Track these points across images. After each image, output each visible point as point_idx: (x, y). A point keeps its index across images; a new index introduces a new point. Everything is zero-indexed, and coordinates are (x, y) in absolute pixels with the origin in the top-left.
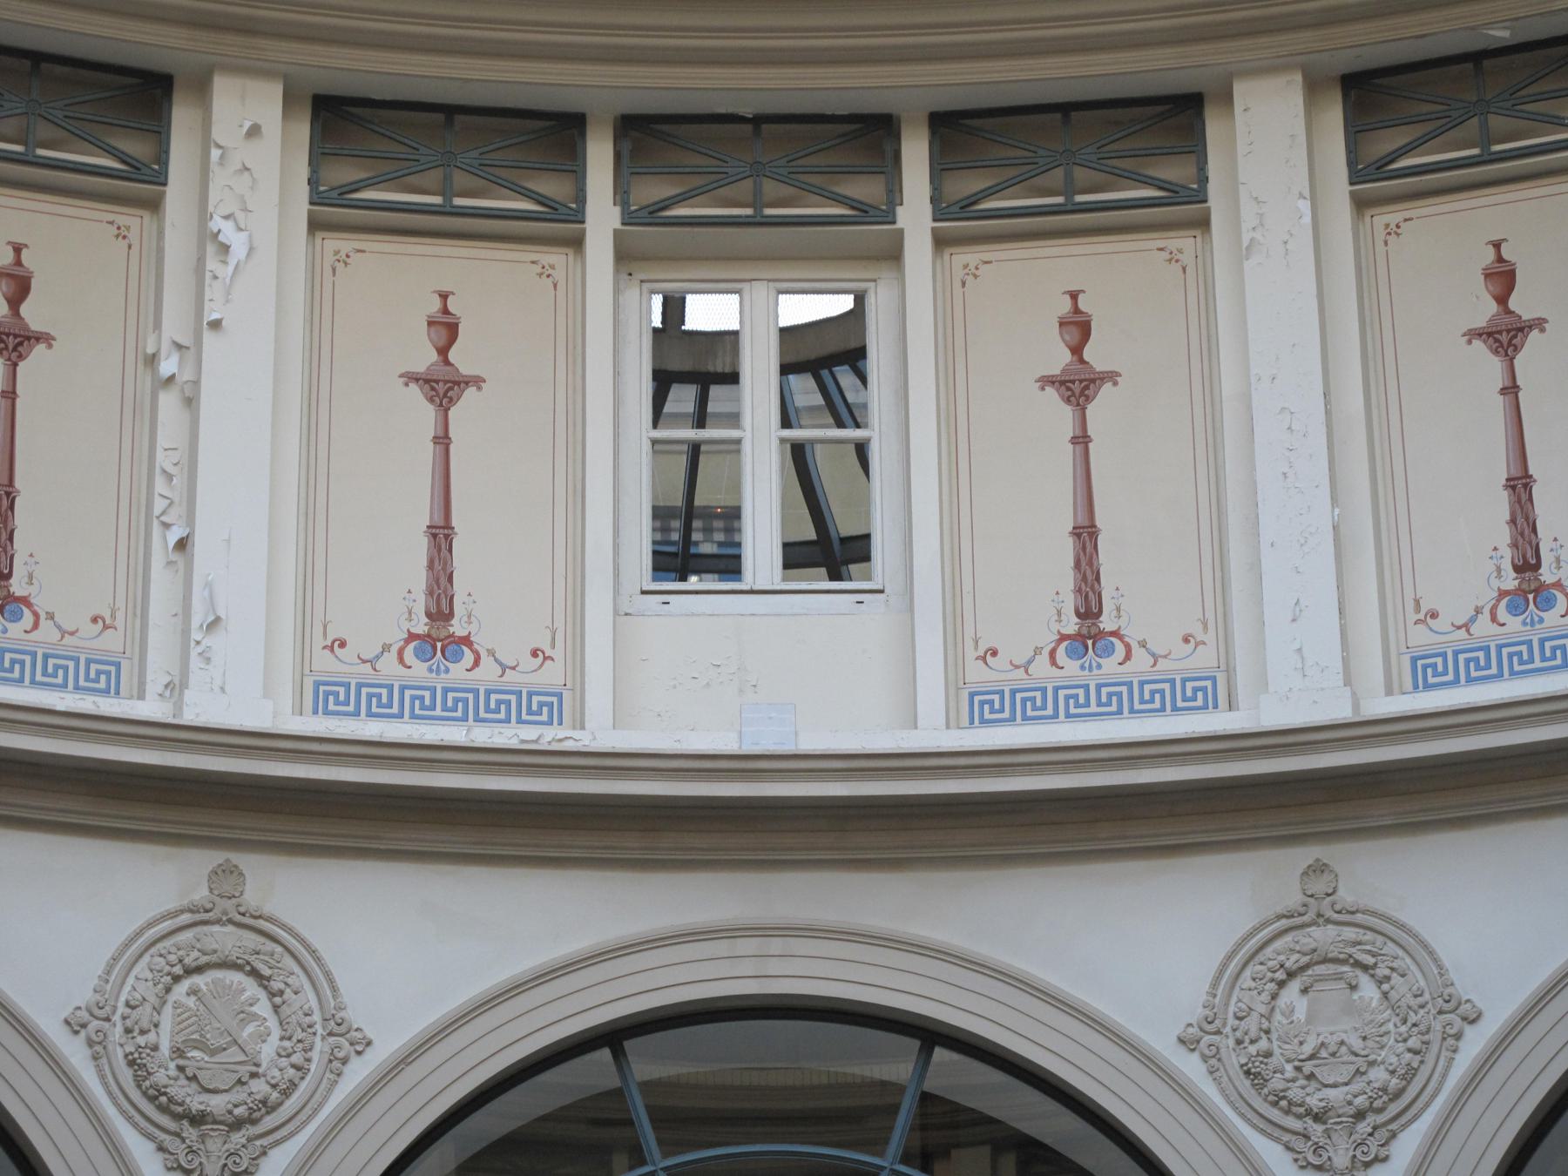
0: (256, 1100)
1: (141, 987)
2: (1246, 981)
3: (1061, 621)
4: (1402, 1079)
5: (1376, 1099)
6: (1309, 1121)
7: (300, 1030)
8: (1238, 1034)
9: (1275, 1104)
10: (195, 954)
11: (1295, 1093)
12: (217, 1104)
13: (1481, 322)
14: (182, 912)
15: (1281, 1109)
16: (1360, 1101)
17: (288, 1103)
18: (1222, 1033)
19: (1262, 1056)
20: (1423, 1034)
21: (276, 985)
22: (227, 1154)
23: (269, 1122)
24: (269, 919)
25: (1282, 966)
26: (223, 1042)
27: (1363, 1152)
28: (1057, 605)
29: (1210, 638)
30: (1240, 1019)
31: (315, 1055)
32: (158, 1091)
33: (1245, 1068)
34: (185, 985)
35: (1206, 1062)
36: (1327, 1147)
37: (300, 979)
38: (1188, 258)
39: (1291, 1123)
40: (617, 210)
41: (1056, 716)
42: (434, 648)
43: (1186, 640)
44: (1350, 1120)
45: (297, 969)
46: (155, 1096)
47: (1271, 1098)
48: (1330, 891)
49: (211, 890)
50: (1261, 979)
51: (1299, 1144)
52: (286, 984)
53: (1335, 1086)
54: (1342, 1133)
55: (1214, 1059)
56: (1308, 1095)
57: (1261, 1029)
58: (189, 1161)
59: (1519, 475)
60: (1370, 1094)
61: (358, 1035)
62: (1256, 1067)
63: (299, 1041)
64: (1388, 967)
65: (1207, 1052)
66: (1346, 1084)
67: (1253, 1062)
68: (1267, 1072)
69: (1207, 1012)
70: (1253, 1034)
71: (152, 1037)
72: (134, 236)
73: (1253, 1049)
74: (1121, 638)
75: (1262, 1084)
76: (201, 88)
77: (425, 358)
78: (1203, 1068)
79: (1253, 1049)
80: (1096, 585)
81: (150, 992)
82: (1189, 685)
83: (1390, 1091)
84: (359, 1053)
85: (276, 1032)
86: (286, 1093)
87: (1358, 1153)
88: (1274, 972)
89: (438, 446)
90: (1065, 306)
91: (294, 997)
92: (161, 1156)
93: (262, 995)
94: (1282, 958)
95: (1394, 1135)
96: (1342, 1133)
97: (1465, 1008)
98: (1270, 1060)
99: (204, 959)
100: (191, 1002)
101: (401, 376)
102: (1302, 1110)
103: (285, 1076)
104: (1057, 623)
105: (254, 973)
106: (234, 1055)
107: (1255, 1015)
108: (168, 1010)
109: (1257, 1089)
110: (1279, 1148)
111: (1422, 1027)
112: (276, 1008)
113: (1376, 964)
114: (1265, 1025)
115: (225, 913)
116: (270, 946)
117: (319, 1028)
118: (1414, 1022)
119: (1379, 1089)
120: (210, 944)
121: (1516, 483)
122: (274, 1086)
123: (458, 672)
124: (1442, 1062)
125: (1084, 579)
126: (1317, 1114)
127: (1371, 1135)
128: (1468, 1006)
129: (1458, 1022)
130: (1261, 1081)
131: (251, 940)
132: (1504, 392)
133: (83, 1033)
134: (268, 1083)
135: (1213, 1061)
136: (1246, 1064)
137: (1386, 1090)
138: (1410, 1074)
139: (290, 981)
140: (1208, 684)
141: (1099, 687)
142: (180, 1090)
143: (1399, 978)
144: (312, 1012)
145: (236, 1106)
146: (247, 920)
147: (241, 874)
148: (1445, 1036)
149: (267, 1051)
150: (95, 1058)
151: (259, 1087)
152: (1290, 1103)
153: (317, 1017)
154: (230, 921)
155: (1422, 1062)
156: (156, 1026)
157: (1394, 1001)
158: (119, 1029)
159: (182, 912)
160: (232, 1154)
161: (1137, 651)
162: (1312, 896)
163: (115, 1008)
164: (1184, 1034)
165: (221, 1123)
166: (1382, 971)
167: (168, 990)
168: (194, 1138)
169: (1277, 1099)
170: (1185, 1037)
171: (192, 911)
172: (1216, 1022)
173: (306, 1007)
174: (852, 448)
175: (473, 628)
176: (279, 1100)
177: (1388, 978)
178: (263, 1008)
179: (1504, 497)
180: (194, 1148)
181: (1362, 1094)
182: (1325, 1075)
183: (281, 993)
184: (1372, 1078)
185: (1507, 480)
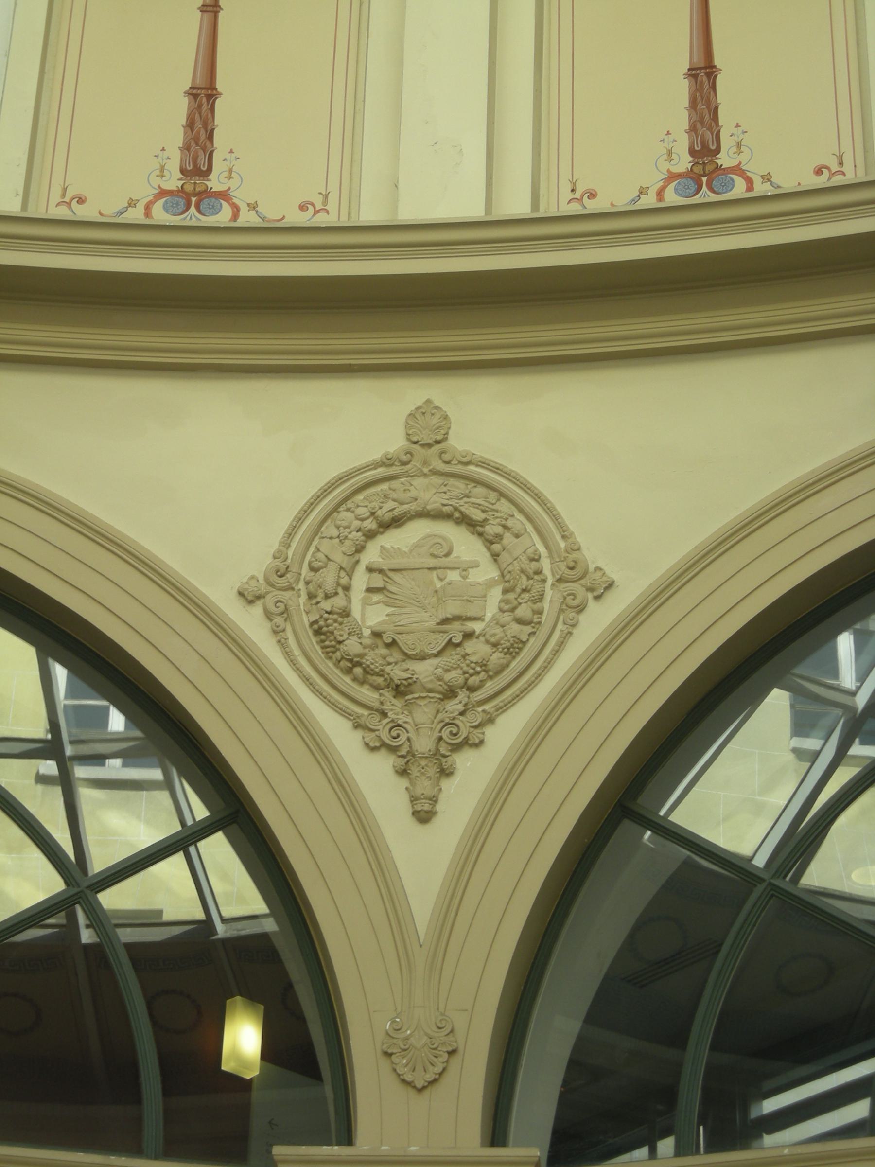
0: (472, 662)
2: (329, 529)
3: (163, 176)
4: (505, 654)
5: (471, 675)
6: (388, 694)
7: (524, 578)
8: (311, 587)
9: (348, 671)
11: (373, 658)
15: (355, 679)
18: (293, 589)
19: (338, 614)
20: (534, 602)
21: (492, 529)
22: (442, 724)
25: (373, 514)
27: (451, 732)
28: (161, 162)
32: (351, 661)
33: (316, 627)
35: (271, 620)
36: (405, 725)
37: (518, 521)
39: (366, 694)
44: (438, 696)
47: (344, 664)
48: (439, 438)
50: (345, 528)
51: (374, 721)
52: (505, 527)
53: (423, 657)
54: (426, 710)
55: (279, 617)
56: (389, 664)
57: (338, 585)
58: (395, 738)
59: (702, 65)
60: (465, 668)
62: (327, 626)
63: (524, 590)
64: (499, 524)
65: (273, 609)
66: (436, 656)
67: (326, 620)
68: (342, 632)
69: (278, 562)
70: (329, 586)
75: (334, 647)
80: (208, 144)
83: (490, 667)
87: (445, 734)
88: (362, 520)
89: (206, 14)
91: (516, 540)
94: (376, 504)
95: (490, 720)
96: (426, 710)
98: (346, 620)
102: (380, 680)
103: (508, 633)
104: (159, 178)
107: (332, 567)
109: (327, 653)
110: (347, 725)
111: (534, 592)
113: (486, 520)
114: (344, 581)
118: (524, 587)
119: (476, 663)
121: (698, 72)
122: (495, 645)
125: (196, 140)
126: (397, 686)
127: (462, 714)
128: (599, 574)
129: (580, 592)
130: (333, 643)
132: (205, 9)
134: (487, 642)
135: (279, 620)
136: (316, 622)
137: (485, 665)
138: (514, 648)
139: (510, 523)
143: (513, 539)
144: (540, 557)
148: (564, 607)
152: (366, 672)
155: (533, 634)
157: (505, 565)
160: (399, 726)
162: (416, 443)
164: (246, 586)
165: (430, 691)
168: (399, 710)
169: (350, 665)
170: (247, 589)
172: (288, 575)
173: (530, 551)
176: (504, 661)
177: (499, 537)
180: (400, 722)
181: (455, 669)
183: (499, 537)
184: (468, 651)
185: (689, 70)
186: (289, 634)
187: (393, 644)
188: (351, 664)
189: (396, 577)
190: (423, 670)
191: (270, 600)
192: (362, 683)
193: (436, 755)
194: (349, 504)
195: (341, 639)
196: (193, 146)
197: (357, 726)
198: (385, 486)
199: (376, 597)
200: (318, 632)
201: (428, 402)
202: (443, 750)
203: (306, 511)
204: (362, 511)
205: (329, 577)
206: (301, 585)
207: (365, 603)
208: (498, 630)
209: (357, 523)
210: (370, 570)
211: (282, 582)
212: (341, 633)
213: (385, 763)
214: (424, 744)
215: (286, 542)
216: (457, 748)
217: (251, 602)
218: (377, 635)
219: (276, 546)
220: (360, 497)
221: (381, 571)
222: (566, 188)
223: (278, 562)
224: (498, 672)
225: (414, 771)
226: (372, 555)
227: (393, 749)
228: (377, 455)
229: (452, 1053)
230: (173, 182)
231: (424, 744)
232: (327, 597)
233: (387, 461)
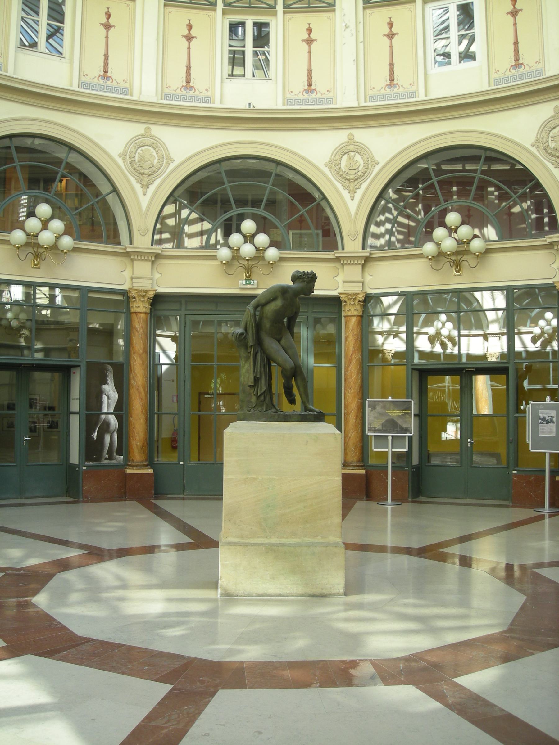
1: (132, 149)
2: (544, 131)
6: (556, 158)
9: (550, 155)
10: (142, 143)
13: (185, 34)
14: (140, 135)
16: (356, 178)
17: (159, 171)
23: (156, 174)
24: (156, 137)
26: (147, 160)
30: (335, 161)
31: (164, 162)
34: (140, 149)
39: (553, 158)
40: (223, 4)
41: (303, 104)
42: (309, 91)
43: (206, 90)
45: (161, 147)
49: (145, 131)
61: (172, 159)
69: (536, 139)
70: (133, 156)
72: (130, 6)
73: (337, 167)
74: (316, 91)
77: (186, 32)
79: (337, 167)
81: (134, 150)
82: (198, 98)
84: (172, 162)
85: (157, 158)
86: (159, 170)
92: (343, 187)
93: (154, 151)
97: (376, 161)
99: (144, 145)
100: (141, 152)
101: (182, 36)
105: (153, 147)
106: (149, 162)
110: (551, 164)
112: (157, 154)
114: (547, 140)
115: (351, 143)
117: (165, 158)
120: (144, 142)
123: (192, 92)
124: (371, 171)
125: (516, 53)
133: (121, 157)
135: (538, 149)
139: (160, 149)
140: (209, 99)
141: (189, 96)
145: (149, 172)
146: (355, 144)
147: (151, 129)
149: (156, 161)
151: (154, 169)
153: (164, 156)
154: (352, 144)
156: (340, 164)
158: (128, 157)
159: (140, 135)
163: (127, 153)
166: (361, 154)
167: (137, 150)
171: (142, 135)
174: (242, 52)
175: (316, 87)
178: (155, 154)
179: (388, 67)
186: (540, 150)
187: (556, 149)
188: (550, 154)
189: (555, 137)
191: (536, 145)
192: (552, 157)
193: (147, 185)
194: (546, 126)
195: (337, 162)
196: (516, 55)
197: (553, 164)
198: (552, 122)
199: (553, 141)
200: (544, 149)
201: (557, 105)
202: (148, 184)
203: (539, 129)
204: (548, 127)
205: (544, 140)
206: (541, 142)
207: (551, 143)
208: (157, 166)
209: (548, 130)
210: (551, 137)
211: (538, 142)
212: (548, 149)
213: (346, 191)
214: (145, 183)
215: (537, 135)
216: (150, 184)
217: (533, 146)
218: (554, 148)
219: (536, 136)
220: (548, 124)
221: (553, 137)
222: (494, 71)
223: (536, 139)
224: (156, 172)
226: (551, 134)
227: (348, 189)
228: (550, 116)
229: (357, 235)
230: (513, 63)
231: (145, 183)
232: (545, 143)
233: (551, 117)
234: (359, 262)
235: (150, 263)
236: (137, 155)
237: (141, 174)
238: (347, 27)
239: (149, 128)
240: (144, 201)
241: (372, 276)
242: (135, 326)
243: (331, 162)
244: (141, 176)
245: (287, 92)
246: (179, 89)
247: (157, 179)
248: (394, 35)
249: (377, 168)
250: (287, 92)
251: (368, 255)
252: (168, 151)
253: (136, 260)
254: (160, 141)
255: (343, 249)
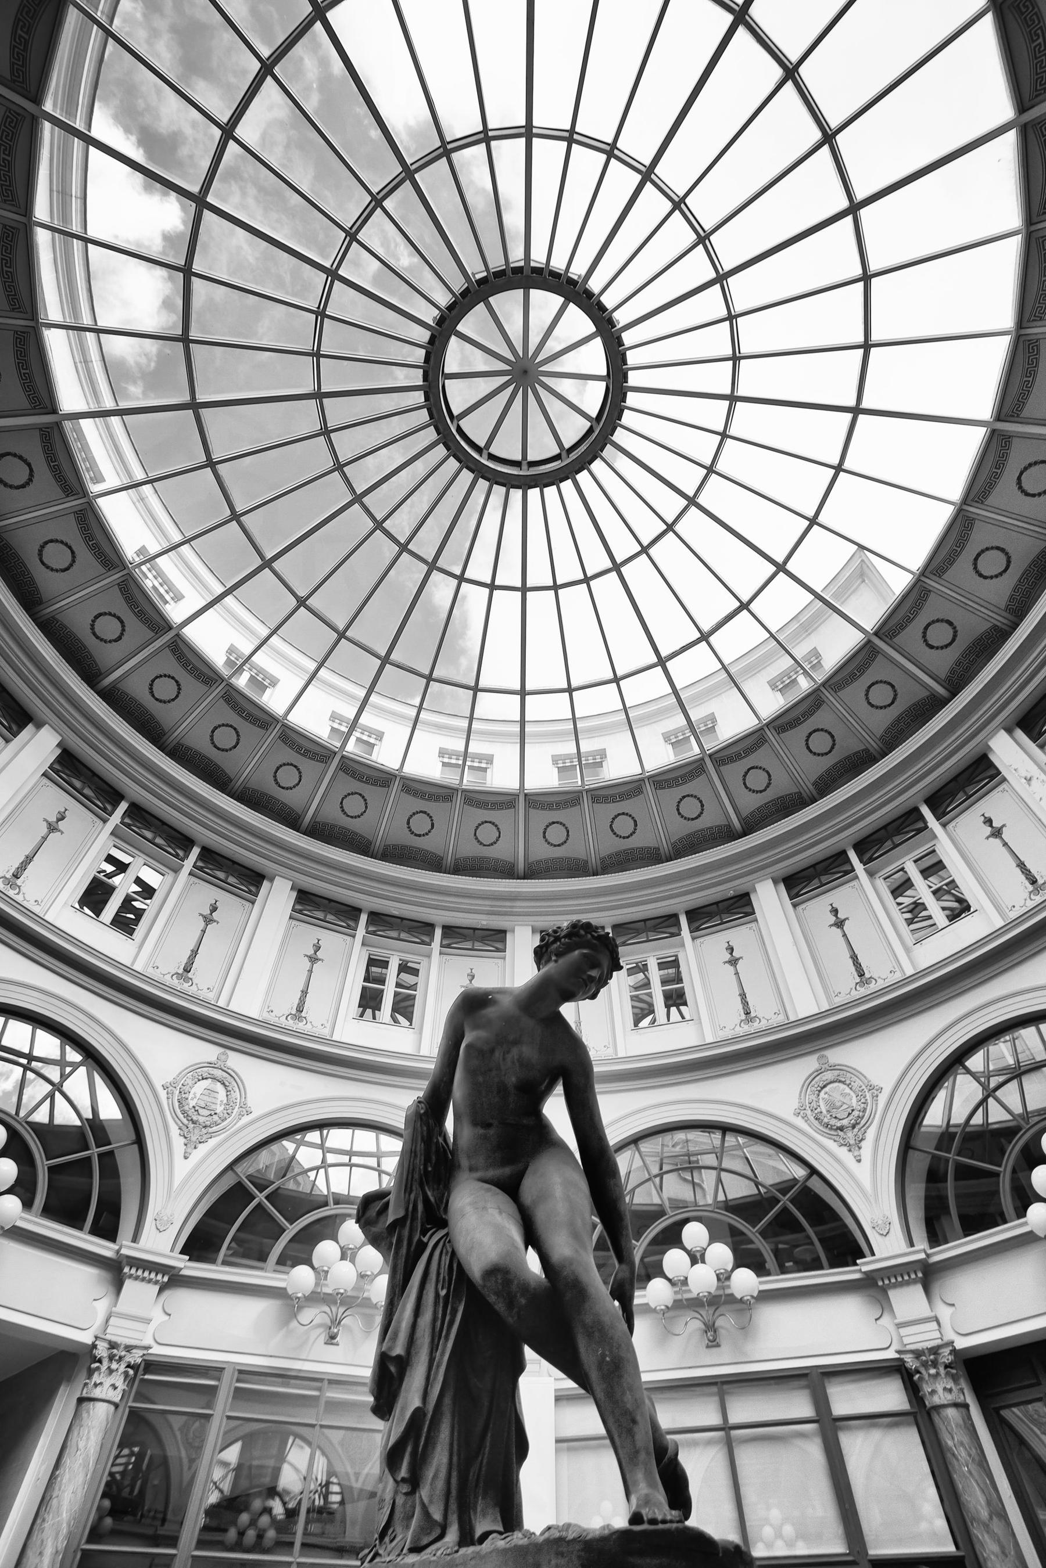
12: (201, 1119)
23: (863, 1122)
24: (838, 1065)
26: (840, 1104)
29: (897, 969)
31: (868, 1097)
37: (854, 1078)
38: (754, 928)
46: (827, 1125)
51: (184, 1128)
71: (819, 1110)
76: (39, 726)
78: (803, 1121)
81: (814, 1097)
85: (854, 1096)
90: (830, 907)
100: (826, 1096)
105: (840, 1081)
106: (845, 1106)
108: (821, 1100)
112: (851, 1089)
116: (842, 1072)
120: (824, 1078)
131: (836, 1073)
142: (833, 1122)
149: (854, 1100)
150: (806, 1121)
151: (856, 1113)
153: (864, 1087)
161: (878, 980)
166: (848, 1082)
178: (847, 1090)
182: (201, 1111)
188: (184, 1112)
190: (845, 1122)
212: (822, 1118)
213: (183, 1140)
214: (852, 1142)
216: (860, 1141)
225: (189, 1146)
227: (186, 1138)
234: (159, 1277)
235: (918, 1289)
236: (822, 1103)
237: (841, 1130)
238: (1029, 780)
239: (823, 1056)
240: (863, 1172)
241: (953, 1305)
242: (947, 1443)
243: (802, 1108)
244: (841, 1133)
245: (1007, 911)
246: (1028, 900)
247: (868, 1127)
248: (737, 959)
249: (883, 1099)
250: (1007, 911)
251: (922, 1256)
252: (865, 1077)
253: (131, 1276)
254: (848, 1069)
255: (873, 1254)
